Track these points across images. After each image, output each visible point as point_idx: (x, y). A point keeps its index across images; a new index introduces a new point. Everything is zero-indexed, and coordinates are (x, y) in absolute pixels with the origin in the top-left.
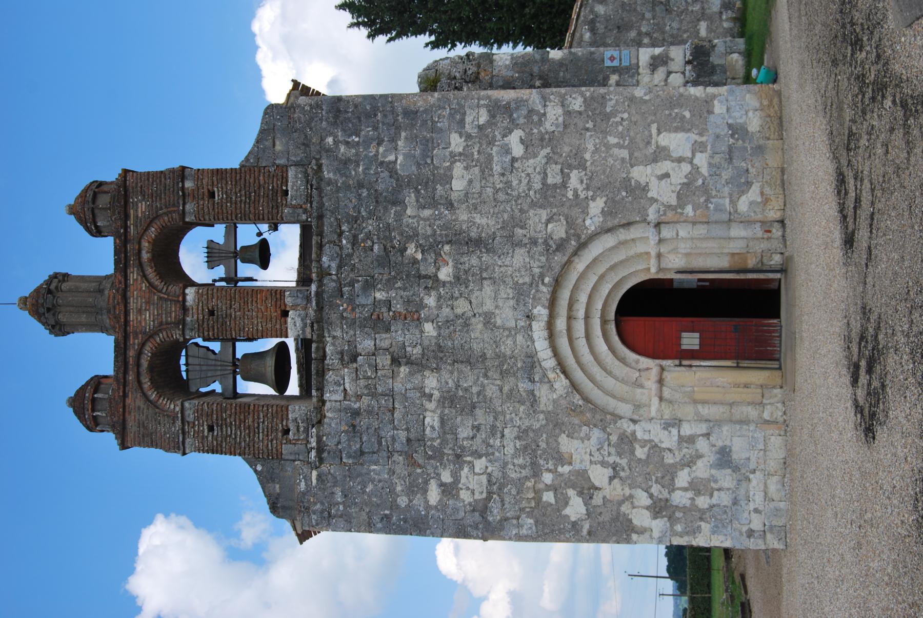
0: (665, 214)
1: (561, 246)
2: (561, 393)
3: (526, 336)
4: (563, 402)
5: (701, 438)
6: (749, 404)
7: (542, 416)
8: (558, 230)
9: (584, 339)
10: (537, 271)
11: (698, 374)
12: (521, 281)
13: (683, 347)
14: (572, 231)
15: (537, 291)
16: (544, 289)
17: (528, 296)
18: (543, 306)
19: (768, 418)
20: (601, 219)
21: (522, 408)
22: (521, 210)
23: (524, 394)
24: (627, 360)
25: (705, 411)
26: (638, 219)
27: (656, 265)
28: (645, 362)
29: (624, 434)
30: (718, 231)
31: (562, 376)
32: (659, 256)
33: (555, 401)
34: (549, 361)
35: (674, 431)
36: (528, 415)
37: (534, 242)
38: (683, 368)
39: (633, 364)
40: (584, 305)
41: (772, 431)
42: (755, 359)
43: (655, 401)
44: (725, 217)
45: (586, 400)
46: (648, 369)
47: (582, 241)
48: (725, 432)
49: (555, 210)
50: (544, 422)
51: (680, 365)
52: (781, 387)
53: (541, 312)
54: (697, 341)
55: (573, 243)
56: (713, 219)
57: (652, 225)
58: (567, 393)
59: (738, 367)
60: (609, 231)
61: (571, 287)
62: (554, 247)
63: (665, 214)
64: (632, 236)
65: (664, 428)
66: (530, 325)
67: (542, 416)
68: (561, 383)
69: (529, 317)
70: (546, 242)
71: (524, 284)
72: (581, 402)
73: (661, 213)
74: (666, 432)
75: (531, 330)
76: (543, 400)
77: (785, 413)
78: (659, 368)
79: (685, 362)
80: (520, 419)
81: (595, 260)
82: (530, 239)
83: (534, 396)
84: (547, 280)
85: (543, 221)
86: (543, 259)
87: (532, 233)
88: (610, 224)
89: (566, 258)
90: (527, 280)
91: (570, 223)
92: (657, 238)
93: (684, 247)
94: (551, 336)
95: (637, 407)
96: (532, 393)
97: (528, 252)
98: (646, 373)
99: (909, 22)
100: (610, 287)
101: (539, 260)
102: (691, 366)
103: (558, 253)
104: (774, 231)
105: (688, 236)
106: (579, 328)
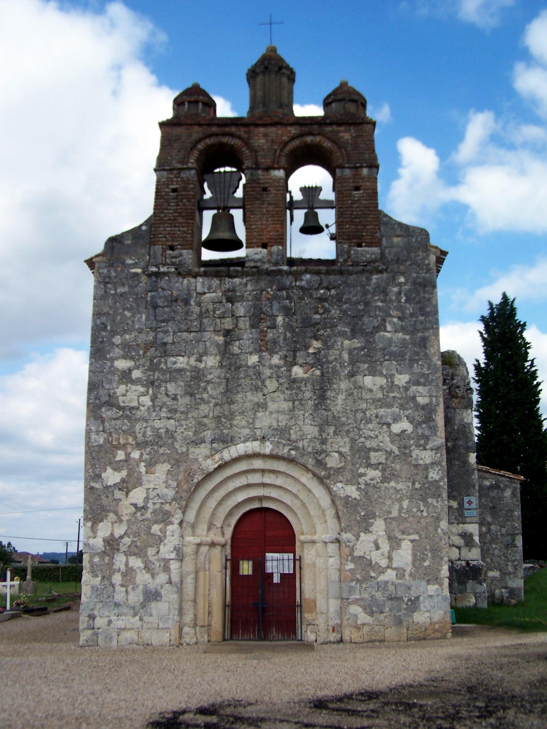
0: (347, 546)
1: (320, 463)
2: (203, 465)
3: (248, 436)
4: (195, 467)
6: (195, 615)
7: (184, 449)
8: (333, 461)
10: (300, 444)
14: (332, 473)
15: (284, 445)
16: (286, 450)
17: (280, 438)
18: (272, 450)
20: (342, 496)
21: (190, 433)
22: (348, 431)
23: (202, 435)
25: (190, 580)
26: (342, 525)
27: (306, 540)
31: (216, 465)
32: (313, 542)
33: (196, 460)
34: (228, 455)
35: (173, 556)
36: (185, 439)
37: (324, 442)
38: (224, 562)
39: (227, 522)
40: (273, 483)
41: (173, 634)
42: (231, 620)
43: (198, 540)
45: (199, 485)
46: (223, 534)
47: (325, 480)
48: (172, 596)
49: (349, 458)
50: (180, 451)
52: (209, 641)
53: (268, 448)
54: (246, 573)
58: (203, 470)
60: (333, 502)
62: (320, 458)
63: (347, 546)
64: (329, 521)
65: (175, 547)
66: (257, 440)
67: (184, 449)
68: (210, 465)
69: (263, 439)
70: (323, 451)
71: (290, 434)
72: (195, 480)
73: (348, 544)
74: (172, 549)
76: (197, 451)
77: (188, 644)
79: (229, 564)
80: (182, 432)
82: (326, 439)
83: (201, 443)
84: (293, 452)
85: (340, 449)
86: (310, 450)
87: (330, 441)
88: (338, 502)
89: (310, 467)
90: (293, 437)
91: (339, 471)
93: (320, 562)
95: (193, 526)
96: (203, 441)
97: (315, 438)
100: (289, 504)
101: (309, 446)
102: (226, 568)
103: (314, 461)
104: (334, 634)
106: (255, 478)
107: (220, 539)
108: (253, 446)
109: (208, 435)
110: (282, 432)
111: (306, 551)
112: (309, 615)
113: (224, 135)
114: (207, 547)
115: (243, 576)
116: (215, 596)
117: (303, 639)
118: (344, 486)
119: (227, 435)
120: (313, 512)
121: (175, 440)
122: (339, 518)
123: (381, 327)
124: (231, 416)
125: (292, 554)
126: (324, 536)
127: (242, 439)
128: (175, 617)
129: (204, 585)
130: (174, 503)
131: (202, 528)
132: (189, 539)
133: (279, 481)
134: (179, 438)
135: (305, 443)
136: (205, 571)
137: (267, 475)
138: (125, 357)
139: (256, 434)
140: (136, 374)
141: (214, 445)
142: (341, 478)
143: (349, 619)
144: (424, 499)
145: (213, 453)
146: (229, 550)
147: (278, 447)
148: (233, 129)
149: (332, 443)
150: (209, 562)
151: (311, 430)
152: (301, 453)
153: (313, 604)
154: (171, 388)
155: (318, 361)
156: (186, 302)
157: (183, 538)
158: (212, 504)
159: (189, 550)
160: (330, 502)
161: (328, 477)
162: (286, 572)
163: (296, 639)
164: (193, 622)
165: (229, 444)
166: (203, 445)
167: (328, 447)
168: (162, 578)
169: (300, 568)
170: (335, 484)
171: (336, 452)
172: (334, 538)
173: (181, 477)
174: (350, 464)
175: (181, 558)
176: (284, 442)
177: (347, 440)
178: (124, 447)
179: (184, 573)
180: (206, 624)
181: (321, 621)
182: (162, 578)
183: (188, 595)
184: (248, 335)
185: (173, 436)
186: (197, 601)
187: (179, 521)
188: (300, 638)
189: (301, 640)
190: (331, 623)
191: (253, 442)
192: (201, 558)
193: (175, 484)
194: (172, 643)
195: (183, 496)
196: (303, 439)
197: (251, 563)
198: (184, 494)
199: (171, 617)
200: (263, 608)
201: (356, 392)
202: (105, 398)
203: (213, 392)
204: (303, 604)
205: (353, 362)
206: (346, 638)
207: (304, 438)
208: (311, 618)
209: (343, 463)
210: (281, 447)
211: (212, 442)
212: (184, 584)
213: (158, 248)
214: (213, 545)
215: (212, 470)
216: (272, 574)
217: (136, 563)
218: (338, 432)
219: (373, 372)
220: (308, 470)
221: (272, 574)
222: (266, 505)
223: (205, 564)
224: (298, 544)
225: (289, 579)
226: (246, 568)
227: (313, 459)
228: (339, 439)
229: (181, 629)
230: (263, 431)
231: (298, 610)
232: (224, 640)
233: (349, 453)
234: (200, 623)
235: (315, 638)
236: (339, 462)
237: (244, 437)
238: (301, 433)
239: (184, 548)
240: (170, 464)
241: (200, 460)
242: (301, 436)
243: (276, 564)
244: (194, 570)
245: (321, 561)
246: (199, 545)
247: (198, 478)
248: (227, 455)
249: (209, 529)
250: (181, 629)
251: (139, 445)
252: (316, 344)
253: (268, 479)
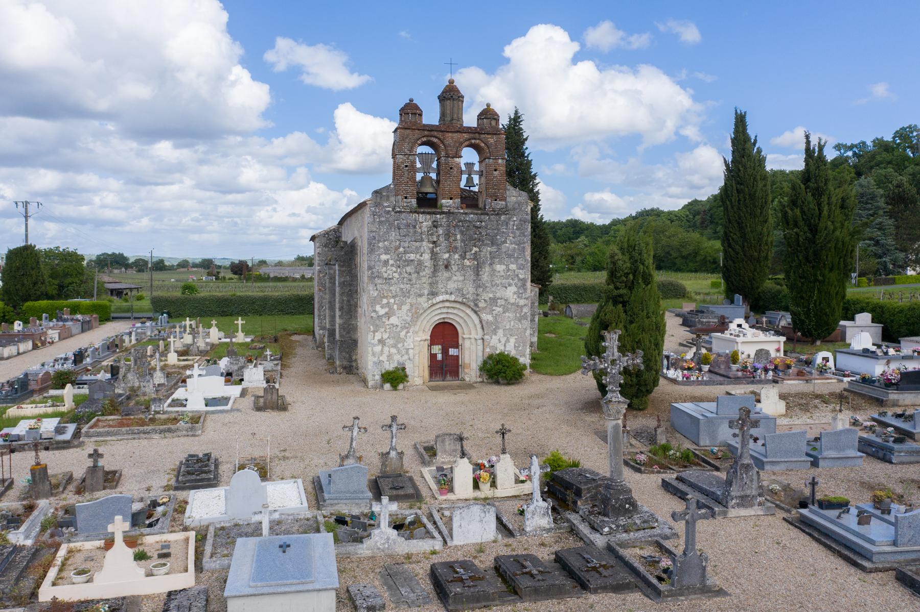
1: (476, 305)
8: (482, 304)
53: (453, 298)
60: (481, 322)
109: (426, 292)
110: (459, 290)
113: (431, 136)
120: (471, 325)
122: (483, 329)
123: (505, 242)
124: (437, 282)
133: (455, 311)
138: (386, 254)
140: (391, 262)
144: (520, 321)
148: (436, 133)
151: (471, 290)
154: (409, 269)
155: (476, 257)
156: (415, 227)
168: (406, 357)
178: (386, 297)
182: (406, 357)
184: (444, 244)
201: (493, 272)
202: (376, 274)
203: (428, 271)
205: (492, 258)
213: (400, 197)
217: (393, 351)
219: (500, 263)
220: (469, 307)
247: (421, 311)
248: (434, 302)
251: (394, 297)
252: (475, 249)
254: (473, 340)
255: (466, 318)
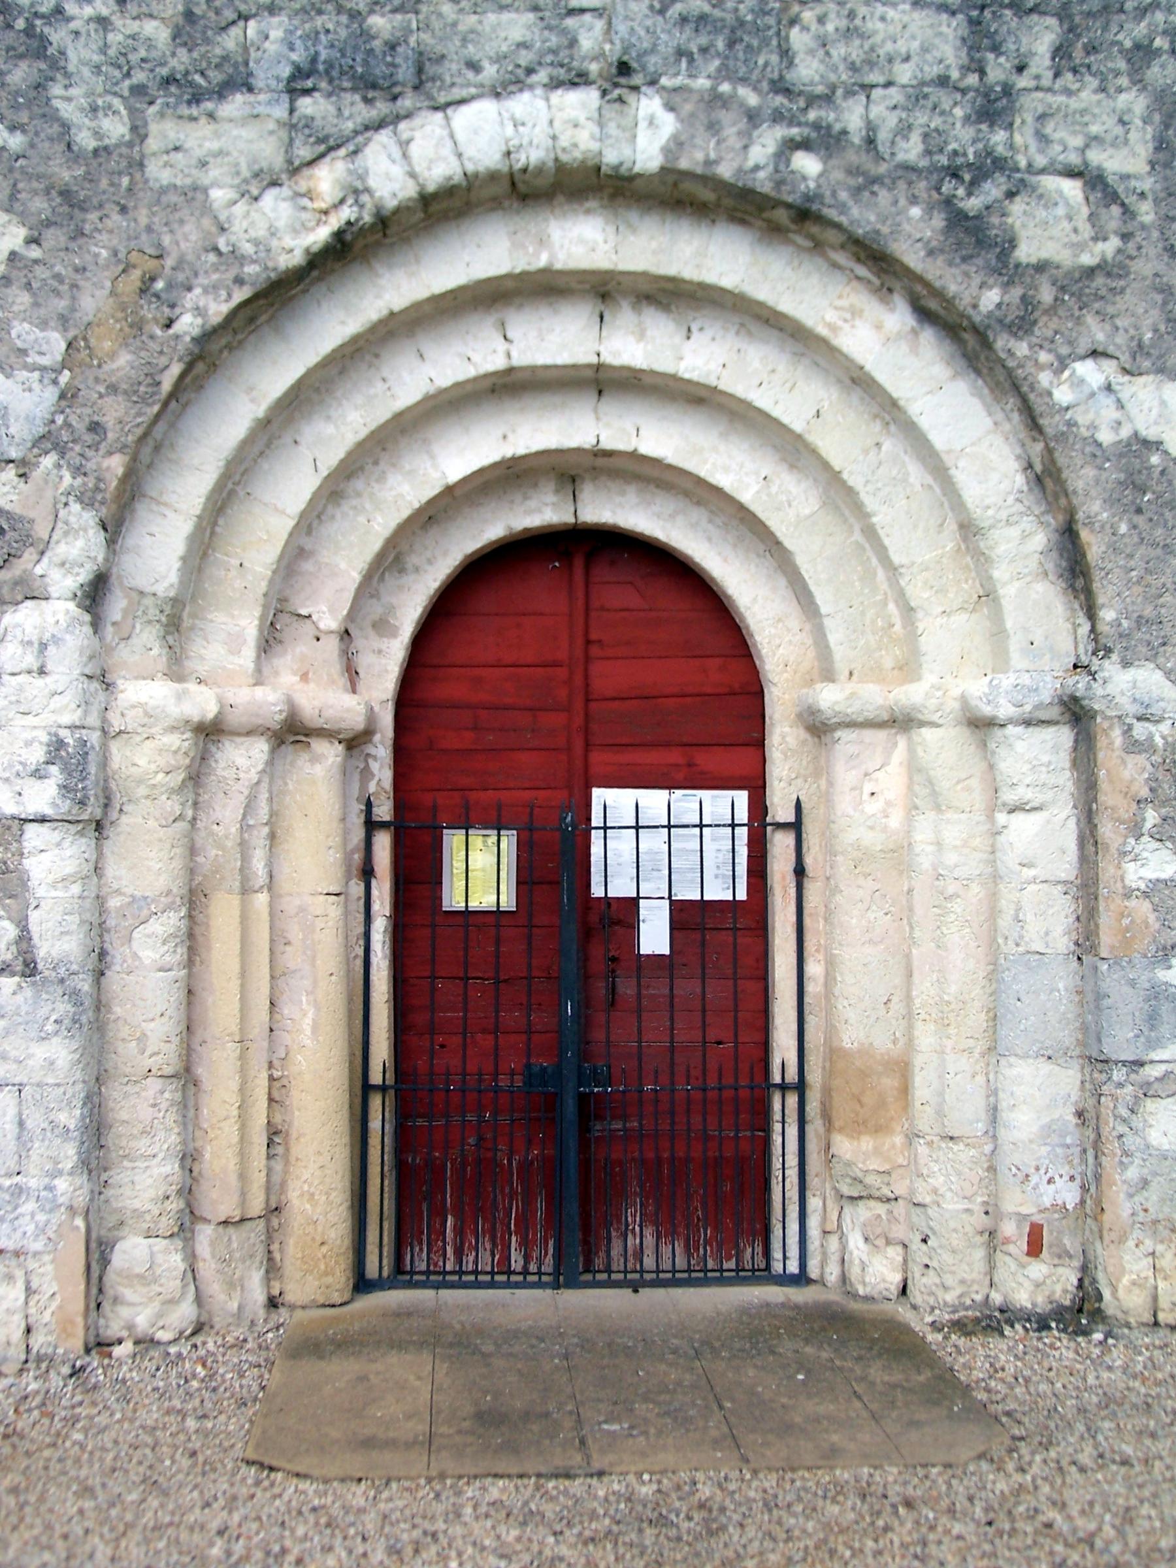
0: (1134, 746)
1: (977, 238)
2: (238, 226)
3: (525, 58)
4: (186, 238)
5: (11, 931)
6: (189, 1159)
7: (116, 128)
8: (1051, 228)
9: (497, 363)
10: (852, 117)
11: (333, 910)
12: (798, 38)
13: (453, 840)
14: (1046, 295)
15: (753, 117)
16: (764, 147)
17: (725, 73)
18: (676, 145)
19: (118, 1259)
20: (1106, 437)
21: (157, 32)
22: (1142, 53)
23: (230, 41)
24: (391, 581)
25: (149, 950)
26: (1107, 615)
27: (853, 710)
28: (386, 662)
29: (27, 540)
30: (1047, 998)
31: (321, 235)
32: (901, 722)
33: (195, 194)
34: (398, 171)
35: (43, 796)
36: (122, 64)
37: (993, 108)
38: (358, 834)
39: (375, 610)
40: (664, 363)
41: (47, 1285)
42: (401, 1167)
43: (202, 703)
44: (1120, 1041)
45: (211, 356)
46: (352, 674)
47: (1002, 342)
48: (41, 1052)
49: (1146, 213)
50: (85, 140)
51: (371, 825)
52: (273, 1303)
53: (648, 135)
54: (483, 900)
55: (991, 298)
56: (1112, 981)
57: (1079, 684)
58: (235, 256)
59: (367, 1088)
60: (1046, 480)
61: (762, 293)
62: (973, 204)
63: (1134, 746)
64: (1008, 592)
65: (58, 745)
66: (579, 80)
67: (116, 128)
68: (287, 229)
69: (622, 76)
70: (992, 164)
71: (786, 54)
72: (188, 324)
73: (1140, 730)
74: (37, 755)
75: (555, 84)
76: (199, 137)
77: (145, 1343)
78: (357, 722)
79: (383, 844)
80: (103, 22)
81: (888, 409)
82: (1008, 90)
83: (222, 91)
84: (808, 164)
85: (1096, 157)
86: (911, 150)
87: (1031, 104)
88: (1082, 478)
89: (913, 258)
90: (807, 71)
91: (1084, 287)
92: (1005, 710)
93: (948, 840)
94: (526, 190)
95: (177, 620)
96: (237, 80)
97: (943, 81)
98: (335, 667)
99: (987, 1282)
100: (746, 497)
101: (904, 130)
102: (367, 873)
103: (939, 221)
104: (1038, 1269)
105: (1009, 860)
106: (556, 338)
107: (332, 702)
108: (553, 123)
111: (845, 775)
112: (867, 1143)
114: (260, 748)
115: (467, 914)
116: (306, 1036)
117: (813, 1271)
118: (1119, 379)
119: (392, 46)
121: (57, 65)
125: (742, 798)
126: (976, 688)
127: (490, 71)
128: (62, 1185)
129: (243, 974)
130: (48, 461)
131: (231, 626)
132: (145, 694)
134: (80, 55)
135: (876, 111)
136: (246, 890)
137: (625, 317)
139: (573, 43)
141: (306, 105)
142: (1098, 333)
143: (1145, 1183)
145: (304, 152)
146: (382, 773)
147: (713, 127)
149: (1042, 118)
150: (272, 836)
152: (853, 171)
153: (890, 1083)
157: (108, 686)
158: (291, 486)
159: (146, 761)
160: (1020, 480)
161: (1022, 326)
162: (717, 892)
163: (764, 1275)
164: (175, 1205)
165: (406, 102)
166: (236, 104)
167: (1019, 141)
169: (800, 872)
170: (1062, 364)
171: (1071, 173)
172: (1046, 696)
173: (93, 301)
174: (1153, 249)
175: (94, 810)
176: (753, 100)
177: (1134, 102)
179: (114, 903)
180: (257, 1205)
181: (947, 1184)
183: (142, 1039)
185: (44, 41)
186: (200, 1071)
187: (84, 575)
188: (793, 1267)
189: (802, 1279)
190: (1021, 1203)
191: (557, 96)
192: (225, 813)
193: (57, 343)
194: (39, 1341)
195: (109, 420)
196: (867, 88)
197: (509, 841)
198: (114, 412)
199: (33, 1183)
200: (583, 1099)
204: (814, 1077)
206: (1124, 1294)
207: (875, 77)
208: (874, 1164)
209: (1114, 242)
210: (731, 130)
211: (298, 84)
212: (114, 979)
214: (292, 733)
215: (297, 259)
216: (631, 905)
218: (1078, 54)
220: (876, 262)
221: (631, 905)
222: (605, 508)
223: (244, 847)
224: (783, 738)
225: (728, 938)
226: (480, 872)
227: (930, 209)
228: (1087, 96)
229: (98, 1254)
230: (622, 28)
231: (783, 1107)
232: (362, 1284)
233: (1147, 185)
234: (220, 1201)
235: (896, 1278)
236: (1087, 231)
237: (499, 59)
238: (855, 50)
239: (118, 753)
240: (23, 217)
241: (218, 195)
242: (853, 68)
243: (656, 847)
244: (178, 888)
245: (952, 834)
246: (210, 732)
247: (204, 307)
249: (270, 639)
250: (98, 1254)
253: (636, 342)
254: (942, 745)
255: (843, 437)
